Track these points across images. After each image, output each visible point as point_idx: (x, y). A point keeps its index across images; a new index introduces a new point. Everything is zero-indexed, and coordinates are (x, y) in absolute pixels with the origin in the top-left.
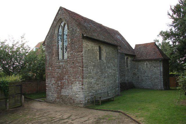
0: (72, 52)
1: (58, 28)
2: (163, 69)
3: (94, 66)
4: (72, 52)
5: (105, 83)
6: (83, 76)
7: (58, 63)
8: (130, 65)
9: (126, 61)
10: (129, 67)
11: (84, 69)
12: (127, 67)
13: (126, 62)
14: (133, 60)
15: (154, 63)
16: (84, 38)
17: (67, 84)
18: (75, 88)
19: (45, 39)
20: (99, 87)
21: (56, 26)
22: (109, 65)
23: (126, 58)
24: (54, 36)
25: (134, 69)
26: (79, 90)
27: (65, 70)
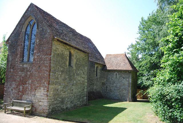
3: (62, 72)
8: (99, 74)
12: (96, 76)
13: (96, 71)
15: (123, 74)
23: (96, 67)
27: (29, 73)
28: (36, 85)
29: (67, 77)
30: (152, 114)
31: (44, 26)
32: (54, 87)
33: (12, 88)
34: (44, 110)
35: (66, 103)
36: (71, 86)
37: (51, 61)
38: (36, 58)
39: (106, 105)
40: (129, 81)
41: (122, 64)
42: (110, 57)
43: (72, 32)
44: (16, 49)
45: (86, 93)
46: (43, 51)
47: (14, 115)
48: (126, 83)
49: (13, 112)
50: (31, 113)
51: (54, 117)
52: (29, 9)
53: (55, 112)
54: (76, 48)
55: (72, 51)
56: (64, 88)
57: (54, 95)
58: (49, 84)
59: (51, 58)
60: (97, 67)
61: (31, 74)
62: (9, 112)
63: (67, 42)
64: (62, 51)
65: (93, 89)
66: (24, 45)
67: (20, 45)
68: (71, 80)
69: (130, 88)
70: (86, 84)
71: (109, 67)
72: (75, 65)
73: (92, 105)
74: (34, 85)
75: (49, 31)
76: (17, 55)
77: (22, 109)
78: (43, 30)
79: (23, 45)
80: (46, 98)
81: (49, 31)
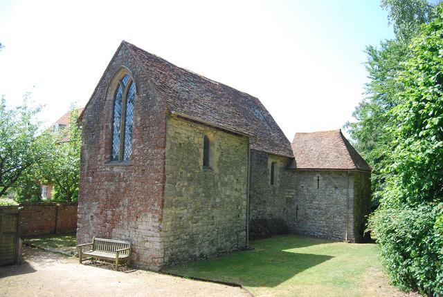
3: (190, 180)
8: (278, 179)
12: (272, 183)
15: (334, 178)
27: (123, 184)
28: (139, 208)
30: (380, 271)
31: (150, 89)
32: (173, 211)
33: (92, 214)
36: (209, 209)
37: (166, 160)
39: (289, 248)
40: (347, 195)
41: (332, 155)
42: (305, 138)
43: (211, 91)
44: (98, 137)
45: (244, 223)
46: (149, 139)
47: (97, 266)
48: (343, 199)
49: (95, 262)
50: (130, 264)
51: (226, 278)
52: (120, 54)
54: (218, 129)
55: (211, 136)
57: (174, 228)
58: (162, 207)
59: (164, 153)
60: (273, 163)
61: (128, 186)
62: (87, 261)
63: (197, 119)
64: (188, 138)
65: (264, 214)
66: (113, 127)
68: (208, 196)
69: (351, 211)
70: (244, 203)
71: (301, 163)
72: (218, 166)
73: (257, 250)
74: (135, 208)
77: (112, 256)
78: (148, 97)
79: (110, 128)
81: (159, 99)
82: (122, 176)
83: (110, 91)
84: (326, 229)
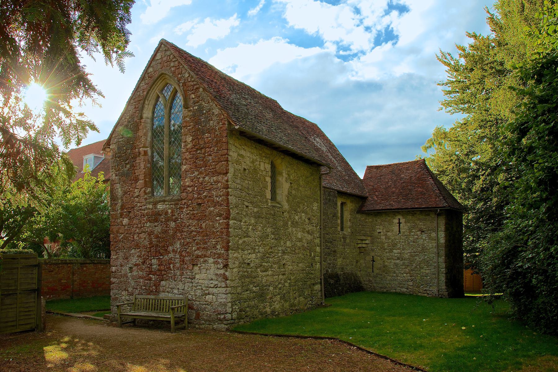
0: (196, 173)
1: (153, 102)
2: (446, 236)
3: (258, 216)
4: (196, 173)
5: (284, 268)
6: (228, 242)
7: (151, 206)
8: (349, 224)
9: (340, 212)
10: (347, 231)
11: (231, 222)
12: (342, 229)
13: (339, 215)
14: (360, 211)
15: (419, 219)
16: (232, 132)
17: (178, 265)
18: (203, 276)
19: (111, 135)
20: (270, 279)
21: (145, 98)
22: (297, 218)
23: (339, 204)
24: (140, 127)
25: (364, 238)
26: (216, 282)
27: (173, 224)
29: (269, 230)
31: (203, 100)
34: (220, 314)
35: (271, 298)
36: (280, 254)
38: (187, 184)
40: (438, 239)
45: (318, 274)
52: (158, 56)
53: (245, 320)
56: (262, 258)
59: (227, 181)
67: (143, 153)
69: (442, 259)
70: (318, 249)
75: (216, 111)
76: (137, 180)
80: (223, 285)
82: (170, 214)
83: (146, 106)
84: (411, 283)
